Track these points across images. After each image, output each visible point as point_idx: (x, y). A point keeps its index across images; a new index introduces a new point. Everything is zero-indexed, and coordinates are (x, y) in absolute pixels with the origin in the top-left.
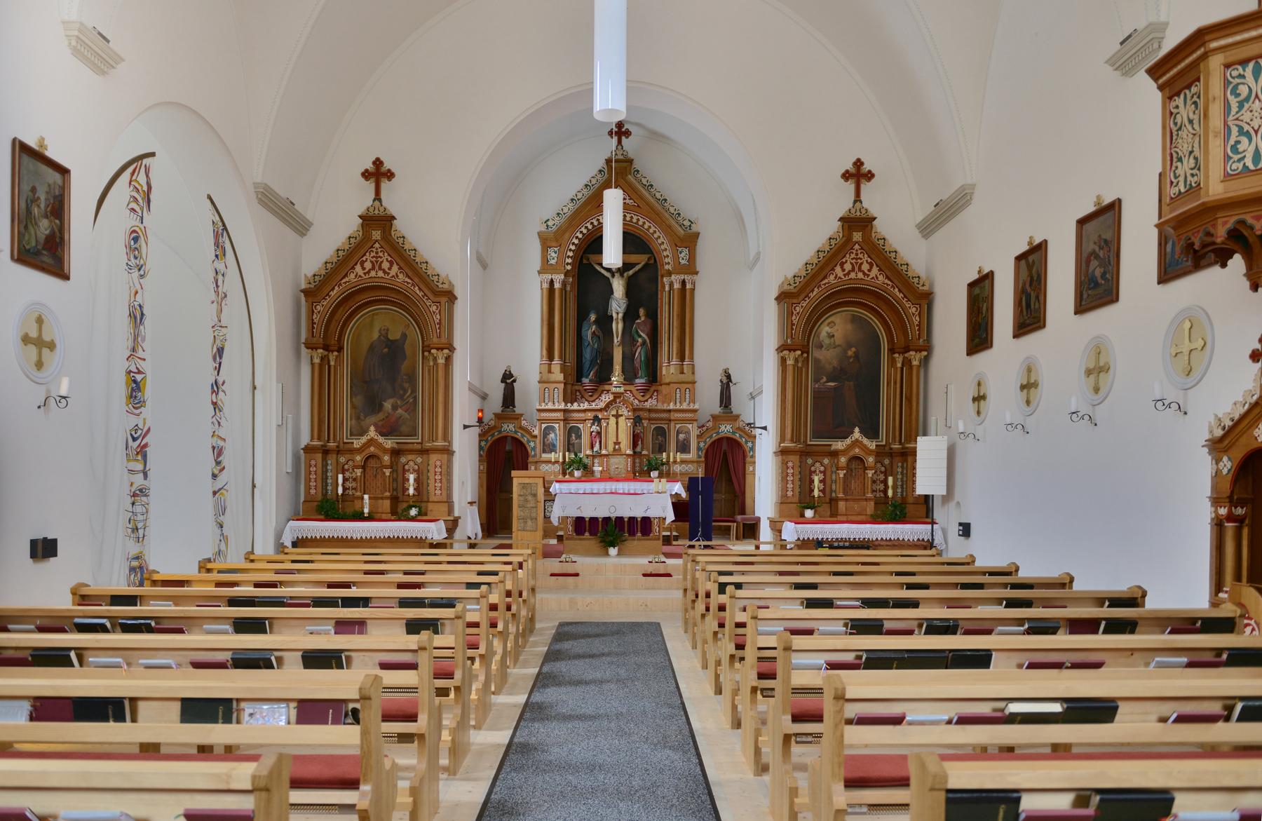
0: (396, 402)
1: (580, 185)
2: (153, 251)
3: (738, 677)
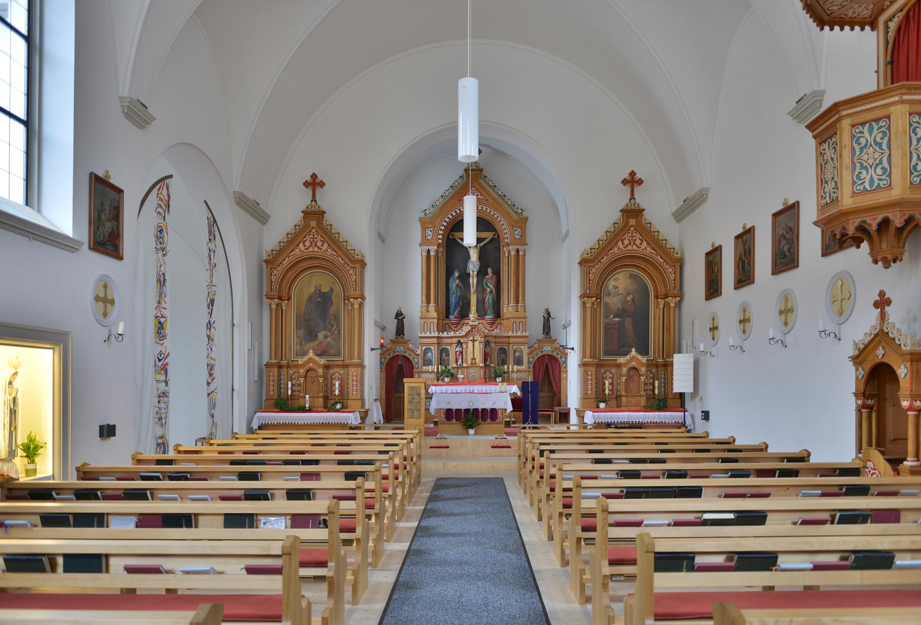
0: (327, 334)
1: (447, 187)
2: (171, 239)
3: (565, 528)
